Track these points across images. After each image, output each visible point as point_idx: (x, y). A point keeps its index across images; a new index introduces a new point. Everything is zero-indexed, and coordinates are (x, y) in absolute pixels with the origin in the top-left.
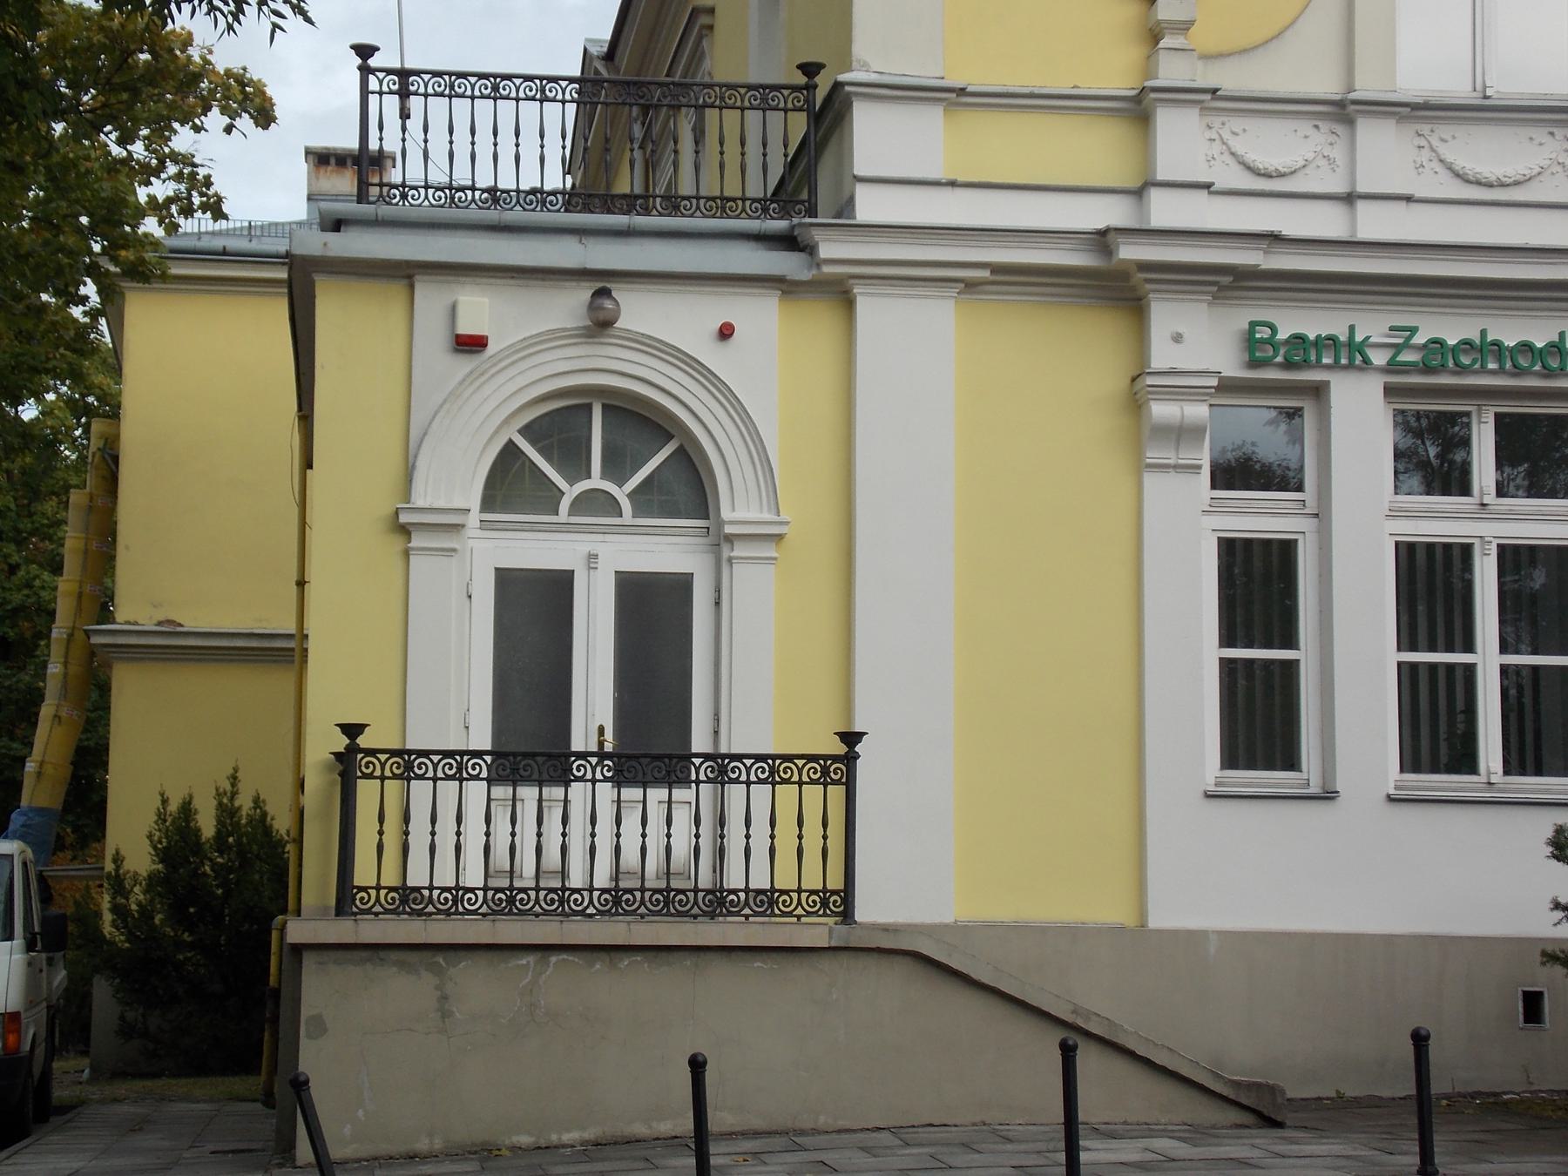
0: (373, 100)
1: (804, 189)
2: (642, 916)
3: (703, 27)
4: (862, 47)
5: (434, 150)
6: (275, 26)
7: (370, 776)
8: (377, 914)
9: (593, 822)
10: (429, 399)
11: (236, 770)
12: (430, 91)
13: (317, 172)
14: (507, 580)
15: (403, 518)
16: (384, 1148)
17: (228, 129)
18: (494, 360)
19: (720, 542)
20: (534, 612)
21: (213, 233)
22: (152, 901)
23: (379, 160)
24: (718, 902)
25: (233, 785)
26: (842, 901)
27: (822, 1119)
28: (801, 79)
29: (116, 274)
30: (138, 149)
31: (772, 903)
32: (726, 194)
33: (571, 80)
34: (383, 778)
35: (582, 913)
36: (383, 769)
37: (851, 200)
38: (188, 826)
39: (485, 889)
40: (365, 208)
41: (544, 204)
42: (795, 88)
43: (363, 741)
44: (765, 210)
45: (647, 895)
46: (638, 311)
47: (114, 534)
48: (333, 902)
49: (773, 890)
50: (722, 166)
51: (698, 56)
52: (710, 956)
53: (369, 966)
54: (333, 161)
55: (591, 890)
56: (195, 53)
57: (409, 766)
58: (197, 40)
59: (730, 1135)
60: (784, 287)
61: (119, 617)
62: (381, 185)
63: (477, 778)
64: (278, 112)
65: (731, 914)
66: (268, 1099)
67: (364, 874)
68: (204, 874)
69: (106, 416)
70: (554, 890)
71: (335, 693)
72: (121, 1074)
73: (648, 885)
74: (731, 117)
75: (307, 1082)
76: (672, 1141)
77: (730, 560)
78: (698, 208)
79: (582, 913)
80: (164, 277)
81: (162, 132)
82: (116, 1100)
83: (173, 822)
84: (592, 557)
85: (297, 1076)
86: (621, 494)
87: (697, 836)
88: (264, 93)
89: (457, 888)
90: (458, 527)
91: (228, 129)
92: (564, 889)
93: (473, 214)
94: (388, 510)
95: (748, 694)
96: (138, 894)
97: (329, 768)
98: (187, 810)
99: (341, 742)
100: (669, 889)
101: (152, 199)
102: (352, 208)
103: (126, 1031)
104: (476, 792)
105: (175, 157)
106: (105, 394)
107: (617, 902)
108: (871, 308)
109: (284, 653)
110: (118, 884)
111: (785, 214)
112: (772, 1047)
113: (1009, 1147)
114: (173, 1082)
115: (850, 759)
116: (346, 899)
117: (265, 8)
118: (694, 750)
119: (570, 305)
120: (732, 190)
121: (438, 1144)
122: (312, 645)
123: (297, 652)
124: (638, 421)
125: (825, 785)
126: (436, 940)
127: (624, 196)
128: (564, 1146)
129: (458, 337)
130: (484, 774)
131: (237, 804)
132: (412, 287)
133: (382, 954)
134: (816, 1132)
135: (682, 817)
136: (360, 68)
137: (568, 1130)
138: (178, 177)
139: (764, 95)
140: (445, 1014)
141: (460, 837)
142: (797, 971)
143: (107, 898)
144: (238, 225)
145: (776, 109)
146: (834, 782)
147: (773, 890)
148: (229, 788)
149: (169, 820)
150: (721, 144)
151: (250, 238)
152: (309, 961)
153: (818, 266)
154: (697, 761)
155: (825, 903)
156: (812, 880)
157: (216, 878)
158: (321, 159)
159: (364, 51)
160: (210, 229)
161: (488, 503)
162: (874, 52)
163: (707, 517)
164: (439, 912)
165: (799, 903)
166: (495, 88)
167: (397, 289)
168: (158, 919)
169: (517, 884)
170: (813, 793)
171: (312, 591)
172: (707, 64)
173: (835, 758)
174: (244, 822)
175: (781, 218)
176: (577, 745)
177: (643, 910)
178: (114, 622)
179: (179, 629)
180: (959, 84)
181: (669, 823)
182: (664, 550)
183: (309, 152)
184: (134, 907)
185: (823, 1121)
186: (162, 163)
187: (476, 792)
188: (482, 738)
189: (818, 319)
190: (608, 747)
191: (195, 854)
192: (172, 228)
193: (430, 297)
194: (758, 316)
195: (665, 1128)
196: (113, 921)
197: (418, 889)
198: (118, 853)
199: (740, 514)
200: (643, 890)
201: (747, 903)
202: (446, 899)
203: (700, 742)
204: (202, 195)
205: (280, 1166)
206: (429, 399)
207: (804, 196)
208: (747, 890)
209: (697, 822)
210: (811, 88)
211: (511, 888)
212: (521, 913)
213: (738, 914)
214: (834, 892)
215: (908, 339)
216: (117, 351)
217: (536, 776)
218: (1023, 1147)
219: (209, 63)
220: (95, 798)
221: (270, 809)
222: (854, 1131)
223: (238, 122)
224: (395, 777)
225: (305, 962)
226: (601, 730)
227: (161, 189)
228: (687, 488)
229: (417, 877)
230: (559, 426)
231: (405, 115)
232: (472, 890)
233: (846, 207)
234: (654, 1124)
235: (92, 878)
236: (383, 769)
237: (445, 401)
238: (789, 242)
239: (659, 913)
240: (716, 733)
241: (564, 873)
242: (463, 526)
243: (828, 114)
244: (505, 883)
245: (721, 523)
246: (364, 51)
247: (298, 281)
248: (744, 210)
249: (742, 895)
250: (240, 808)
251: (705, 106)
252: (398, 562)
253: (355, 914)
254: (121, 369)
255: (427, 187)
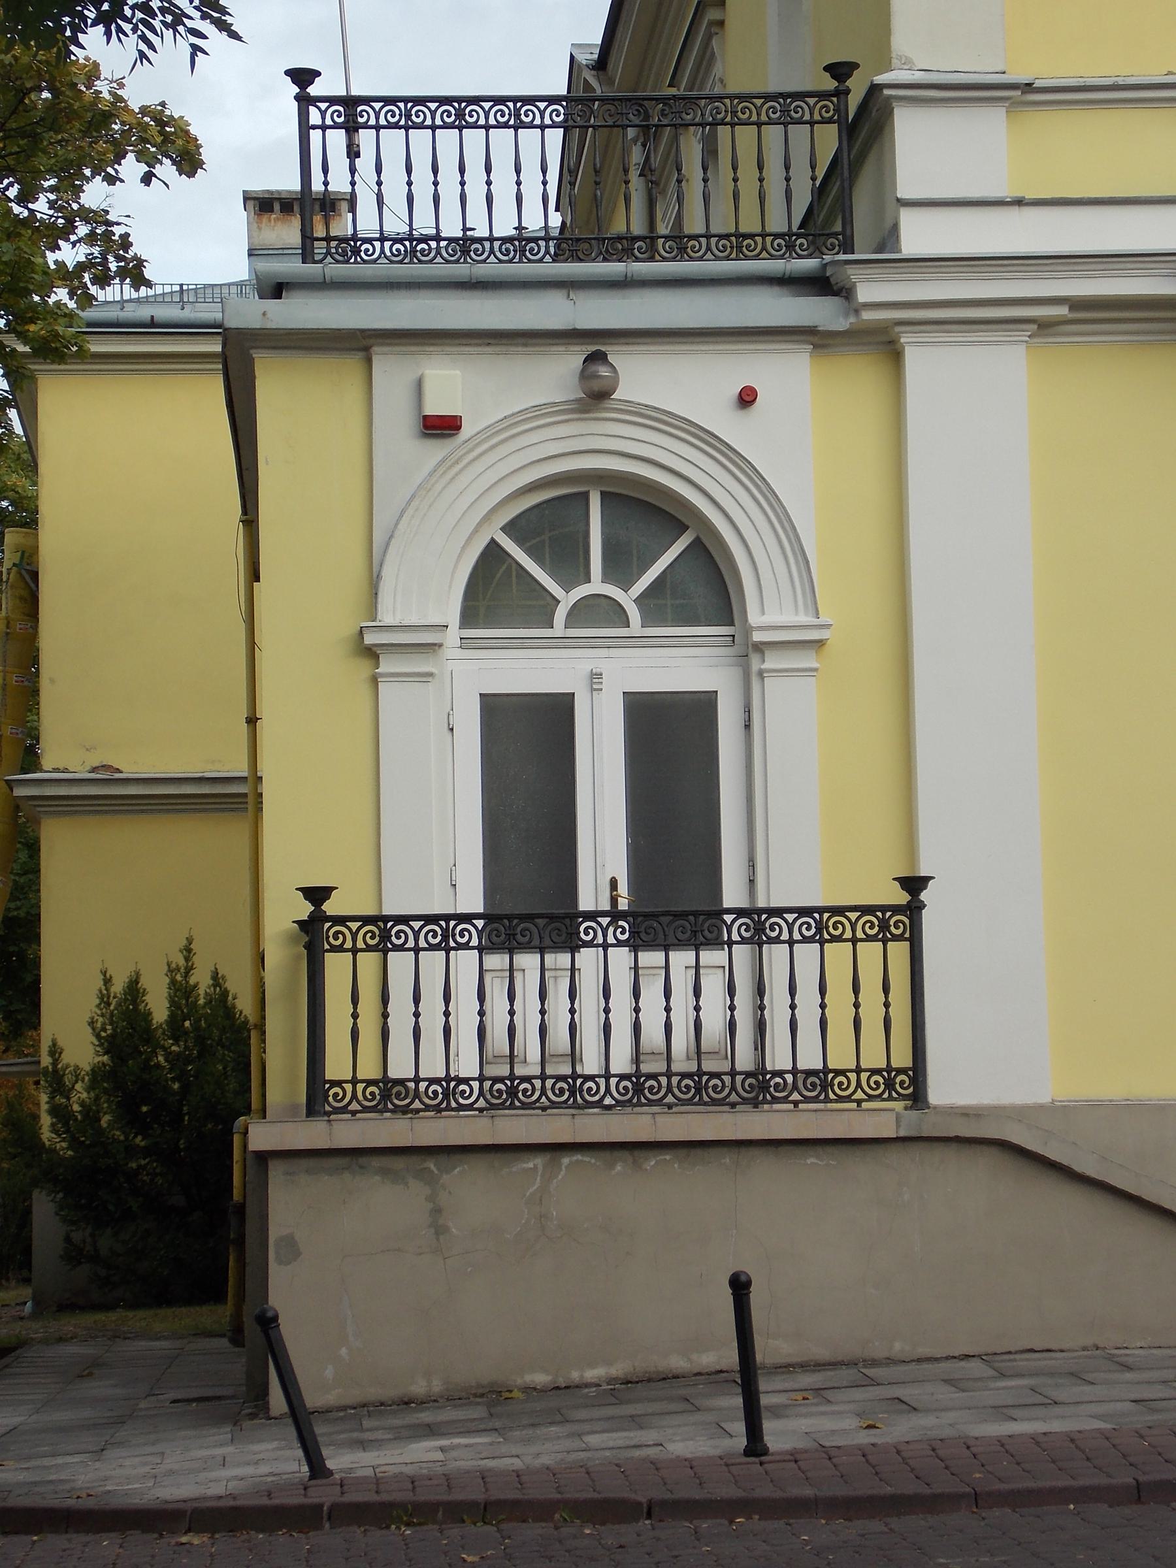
0: (315, 136)
1: (837, 220)
2: (670, 1106)
3: (712, 23)
4: (903, 41)
5: (395, 190)
6: (196, 49)
7: (340, 949)
8: (354, 1113)
9: (607, 994)
10: (405, 486)
11: (190, 941)
12: (383, 122)
13: (259, 222)
14: (494, 708)
15: (369, 639)
16: (373, 1393)
17: (147, 179)
18: (470, 445)
19: (747, 652)
20: (528, 743)
21: (138, 301)
22: (97, 1098)
23: (328, 204)
24: (761, 1086)
25: (187, 959)
26: (912, 1082)
27: (897, 1346)
28: (830, 84)
29: (24, 355)
30: (41, 205)
31: (826, 1086)
32: (742, 230)
33: (552, 100)
34: (355, 951)
35: (599, 1104)
36: (354, 940)
37: (895, 228)
38: (136, 1009)
39: (481, 1079)
40: (311, 270)
41: (523, 252)
42: (822, 95)
43: (331, 907)
44: (790, 247)
45: (675, 1080)
46: (639, 377)
47: (35, 661)
48: (303, 1099)
49: (826, 1070)
50: (736, 196)
51: (707, 59)
52: (755, 1152)
53: (347, 1176)
54: (277, 207)
55: (607, 1076)
56: (102, 87)
57: (385, 936)
58: (105, 72)
59: (787, 1368)
60: (816, 339)
61: (48, 762)
62: (328, 239)
63: (466, 946)
64: (205, 154)
65: (776, 1100)
66: (237, 1336)
67: (336, 1066)
68: (158, 1065)
69: (24, 525)
70: (563, 1078)
71: (297, 848)
72: (67, 1307)
73: (675, 1068)
74: (747, 135)
75: (275, 1318)
76: (715, 1376)
77: (761, 674)
78: (709, 249)
79: (599, 1104)
80: (83, 355)
81: (71, 185)
82: (60, 1340)
83: (119, 1005)
84: (595, 677)
85: (264, 1312)
86: (627, 599)
87: (732, 1008)
88: (187, 132)
89: (448, 1078)
90: (433, 648)
91: (147, 179)
92: (575, 1076)
93: (439, 270)
94: (351, 629)
95: (789, 833)
96: (80, 1093)
97: (292, 939)
98: (134, 990)
99: (305, 909)
100: (700, 1073)
101: (60, 265)
102: (293, 267)
103: (73, 1255)
104: (466, 962)
105: (87, 215)
106: (22, 498)
107: (638, 1089)
108: (922, 359)
109: (233, 800)
110: (57, 1081)
111: (816, 250)
112: (834, 1262)
113: (1129, 1376)
114: (130, 1314)
115: (914, 909)
116: (318, 1096)
117: (181, 28)
118: (726, 905)
119: (557, 374)
120: (749, 224)
121: (437, 1387)
122: (267, 789)
123: (250, 799)
124: (646, 512)
125: (885, 942)
126: (430, 1141)
127: (619, 238)
128: (587, 1385)
129: (425, 417)
130: (475, 942)
131: (192, 981)
132: (369, 361)
133: (363, 1160)
134: (890, 1361)
135: (713, 985)
136: (297, 98)
137: (592, 1365)
138: (91, 239)
139: (785, 106)
140: (440, 1230)
141: (445, 1017)
142: (860, 1166)
143: (44, 1098)
144: (168, 289)
145: (800, 122)
146: (896, 938)
147: (826, 1070)
148: (182, 962)
149: (114, 1002)
150: (735, 169)
151: (183, 304)
152: (276, 1172)
153: (857, 312)
154: (728, 918)
155: (890, 1085)
156: (874, 1057)
157: (171, 1070)
158: (263, 205)
159: (302, 77)
160: (135, 295)
161: (469, 617)
162: (922, 40)
163: (732, 624)
164: (428, 1108)
165: (859, 1085)
166: (460, 115)
167: (351, 365)
168: (105, 1120)
169: (519, 1071)
170: (870, 952)
171: (265, 728)
172: (718, 70)
173: (896, 909)
174: (201, 1002)
175: (809, 256)
176: (586, 903)
177: (670, 1099)
178: (42, 771)
179: (117, 776)
180: (1023, 78)
181: (697, 993)
182: (681, 665)
183: (247, 197)
184: (76, 1107)
185: (898, 1348)
186: (70, 227)
187: (466, 962)
188: (472, 900)
189: (858, 376)
190: (623, 905)
191: (147, 1041)
192: (87, 300)
193: (392, 373)
194: (784, 375)
195: (708, 1360)
196: (53, 1125)
197: (401, 1082)
198: (54, 1044)
199: (771, 618)
200: (669, 1074)
201: (795, 1087)
202: (435, 1093)
203: (732, 895)
204: (119, 259)
205: (253, 1416)
206: (405, 486)
207: (838, 227)
208: (794, 1071)
209: (731, 990)
210: (842, 93)
211: (512, 1077)
212: (525, 1106)
213: (785, 1100)
214: (900, 1071)
215: (967, 392)
216: (31, 444)
217: (536, 942)
218: (1146, 1375)
219: (120, 99)
220: (29, 978)
221: (231, 986)
222: (937, 1360)
223: (158, 170)
224: (369, 948)
225: (271, 1174)
226: (614, 884)
227: (69, 254)
228: (706, 589)
229: (400, 1068)
230: (549, 521)
231: (353, 153)
232: (466, 1081)
233: (889, 237)
234: (695, 1357)
235: (29, 1074)
236: (354, 940)
237: (413, 497)
238: (820, 284)
239: (689, 1102)
240: (752, 882)
241: (574, 1056)
242: (440, 645)
243: (862, 123)
244: (504, 1071)
245: (748, 630)
246: (302, 77)
247: (235, 360)
248: (764, 248)
249: (789, 1078)
250: (196, 985)
251: (714, 124)
252: (365, 691)
253: (328, 1114)
254: (36, 465)
255: (382, 239)
